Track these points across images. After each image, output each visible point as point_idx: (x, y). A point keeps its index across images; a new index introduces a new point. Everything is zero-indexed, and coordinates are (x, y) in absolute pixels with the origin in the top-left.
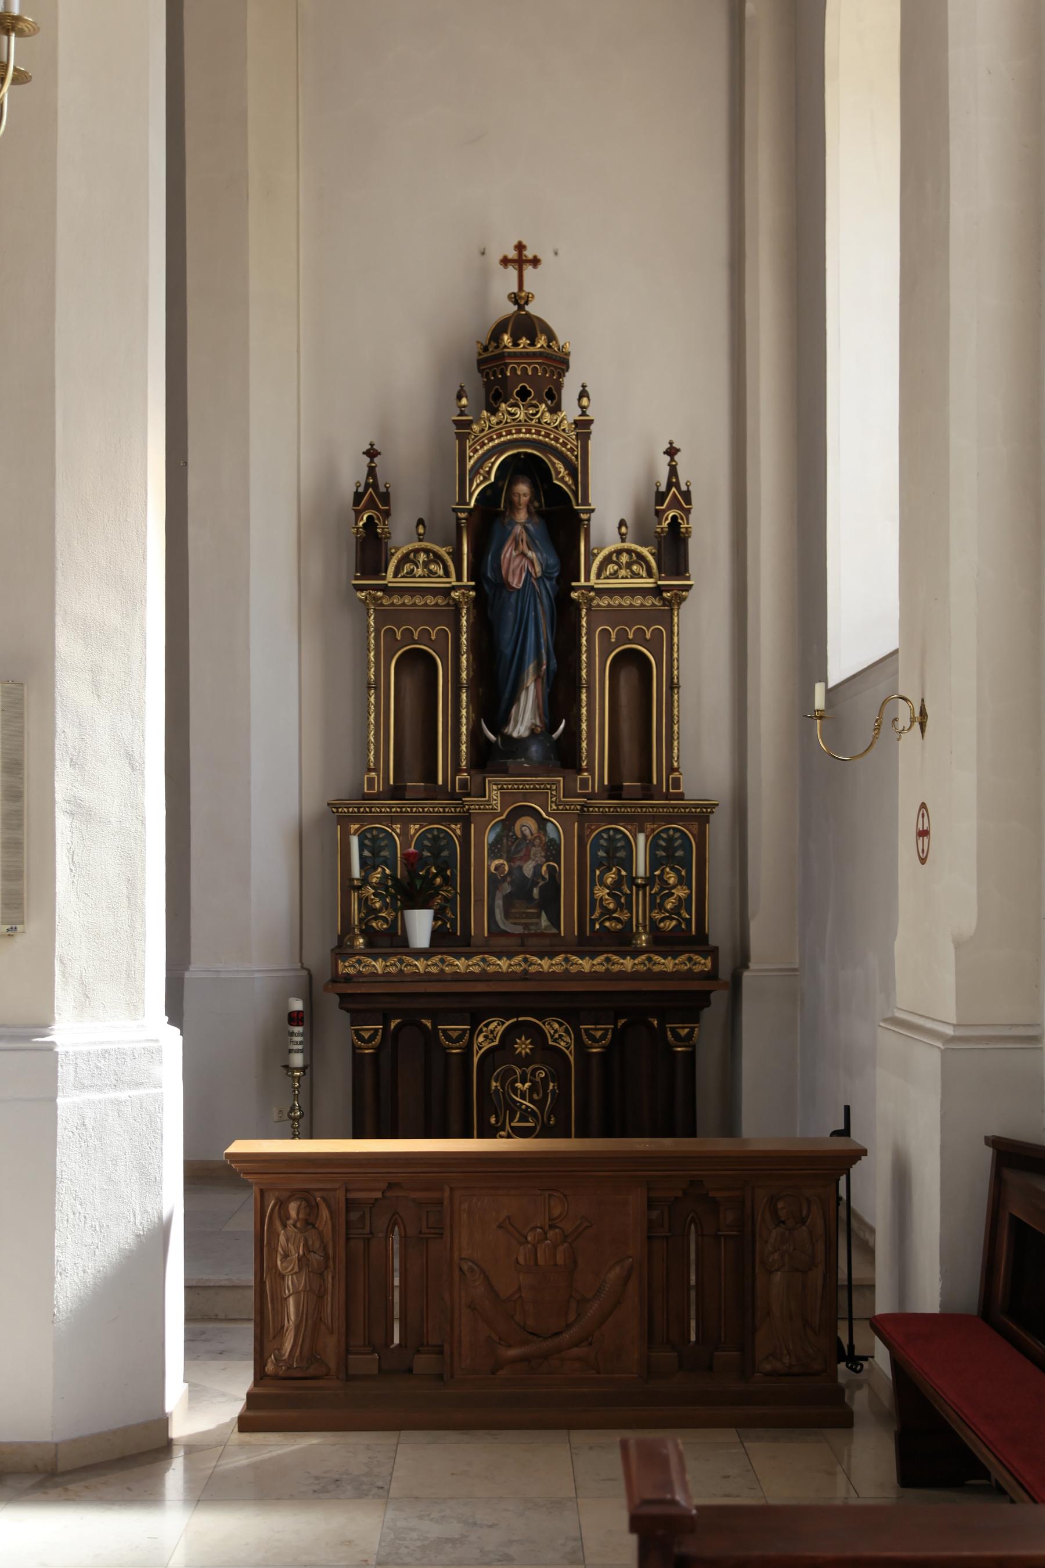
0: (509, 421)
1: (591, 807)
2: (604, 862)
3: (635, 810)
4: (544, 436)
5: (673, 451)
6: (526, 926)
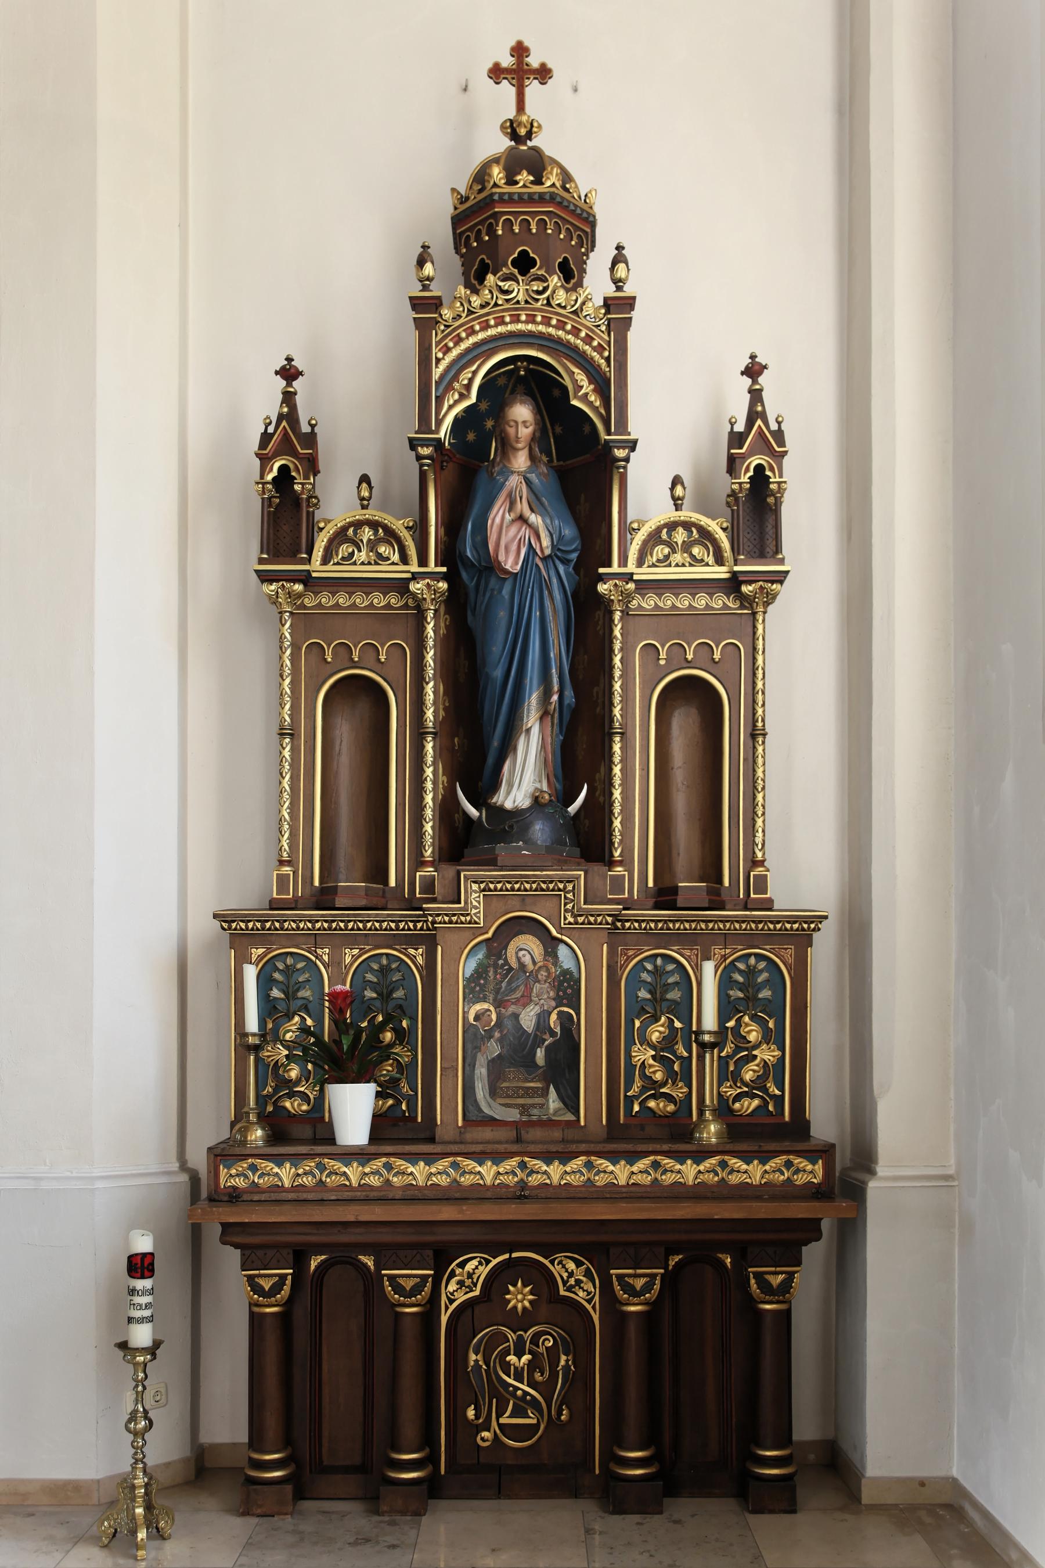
0: (500, 302)
1: (627, 921)
2: (647, 1008)
3: (696, 926)
4: (556, 327)
5: (756, 367)
6: (524, 1109)
